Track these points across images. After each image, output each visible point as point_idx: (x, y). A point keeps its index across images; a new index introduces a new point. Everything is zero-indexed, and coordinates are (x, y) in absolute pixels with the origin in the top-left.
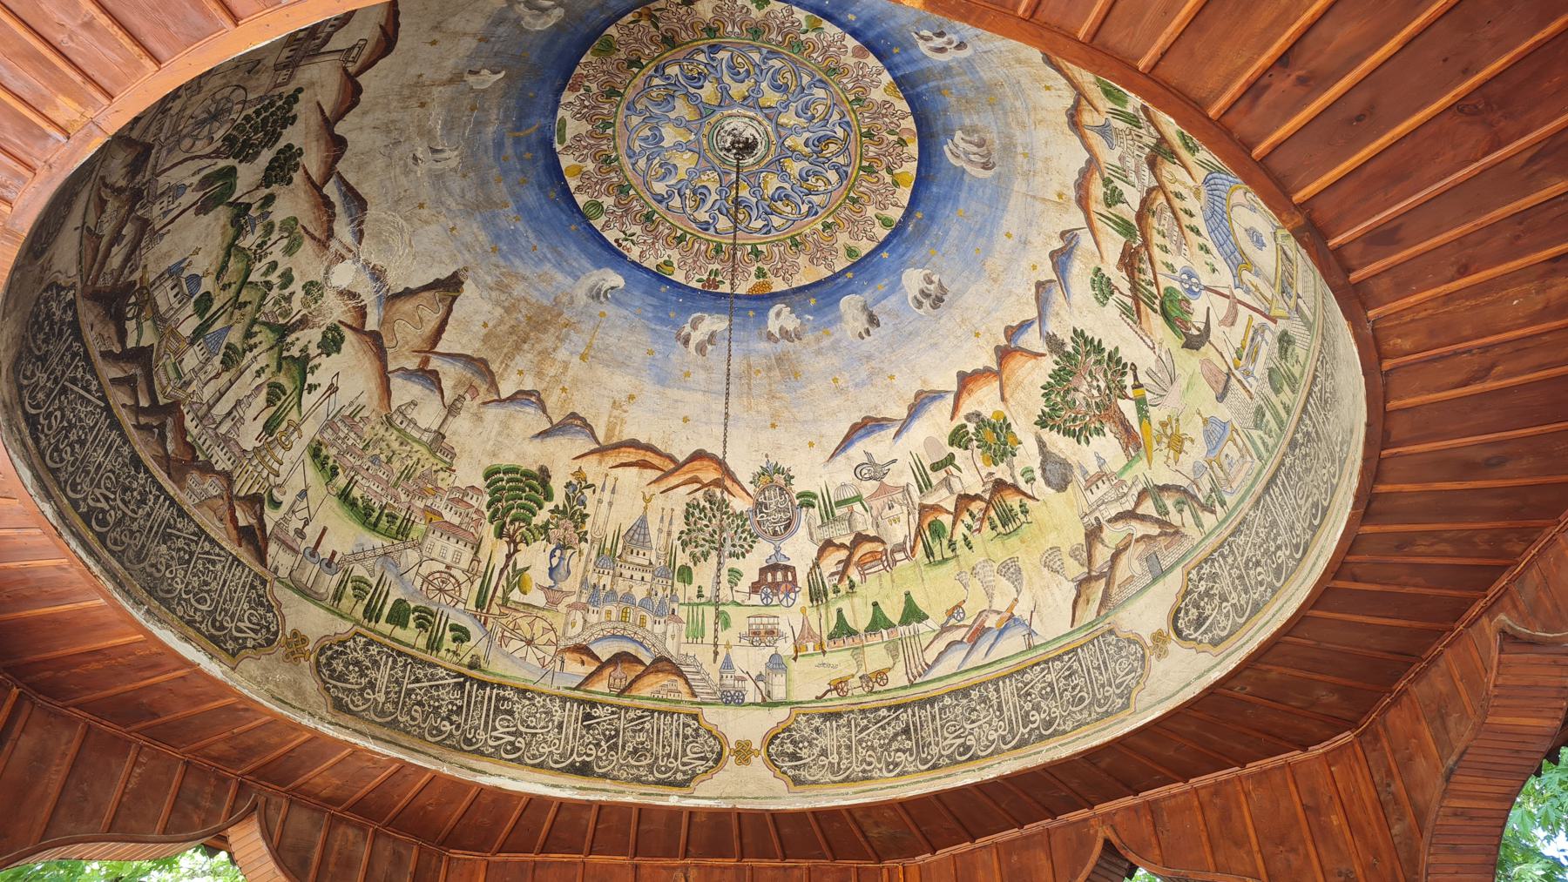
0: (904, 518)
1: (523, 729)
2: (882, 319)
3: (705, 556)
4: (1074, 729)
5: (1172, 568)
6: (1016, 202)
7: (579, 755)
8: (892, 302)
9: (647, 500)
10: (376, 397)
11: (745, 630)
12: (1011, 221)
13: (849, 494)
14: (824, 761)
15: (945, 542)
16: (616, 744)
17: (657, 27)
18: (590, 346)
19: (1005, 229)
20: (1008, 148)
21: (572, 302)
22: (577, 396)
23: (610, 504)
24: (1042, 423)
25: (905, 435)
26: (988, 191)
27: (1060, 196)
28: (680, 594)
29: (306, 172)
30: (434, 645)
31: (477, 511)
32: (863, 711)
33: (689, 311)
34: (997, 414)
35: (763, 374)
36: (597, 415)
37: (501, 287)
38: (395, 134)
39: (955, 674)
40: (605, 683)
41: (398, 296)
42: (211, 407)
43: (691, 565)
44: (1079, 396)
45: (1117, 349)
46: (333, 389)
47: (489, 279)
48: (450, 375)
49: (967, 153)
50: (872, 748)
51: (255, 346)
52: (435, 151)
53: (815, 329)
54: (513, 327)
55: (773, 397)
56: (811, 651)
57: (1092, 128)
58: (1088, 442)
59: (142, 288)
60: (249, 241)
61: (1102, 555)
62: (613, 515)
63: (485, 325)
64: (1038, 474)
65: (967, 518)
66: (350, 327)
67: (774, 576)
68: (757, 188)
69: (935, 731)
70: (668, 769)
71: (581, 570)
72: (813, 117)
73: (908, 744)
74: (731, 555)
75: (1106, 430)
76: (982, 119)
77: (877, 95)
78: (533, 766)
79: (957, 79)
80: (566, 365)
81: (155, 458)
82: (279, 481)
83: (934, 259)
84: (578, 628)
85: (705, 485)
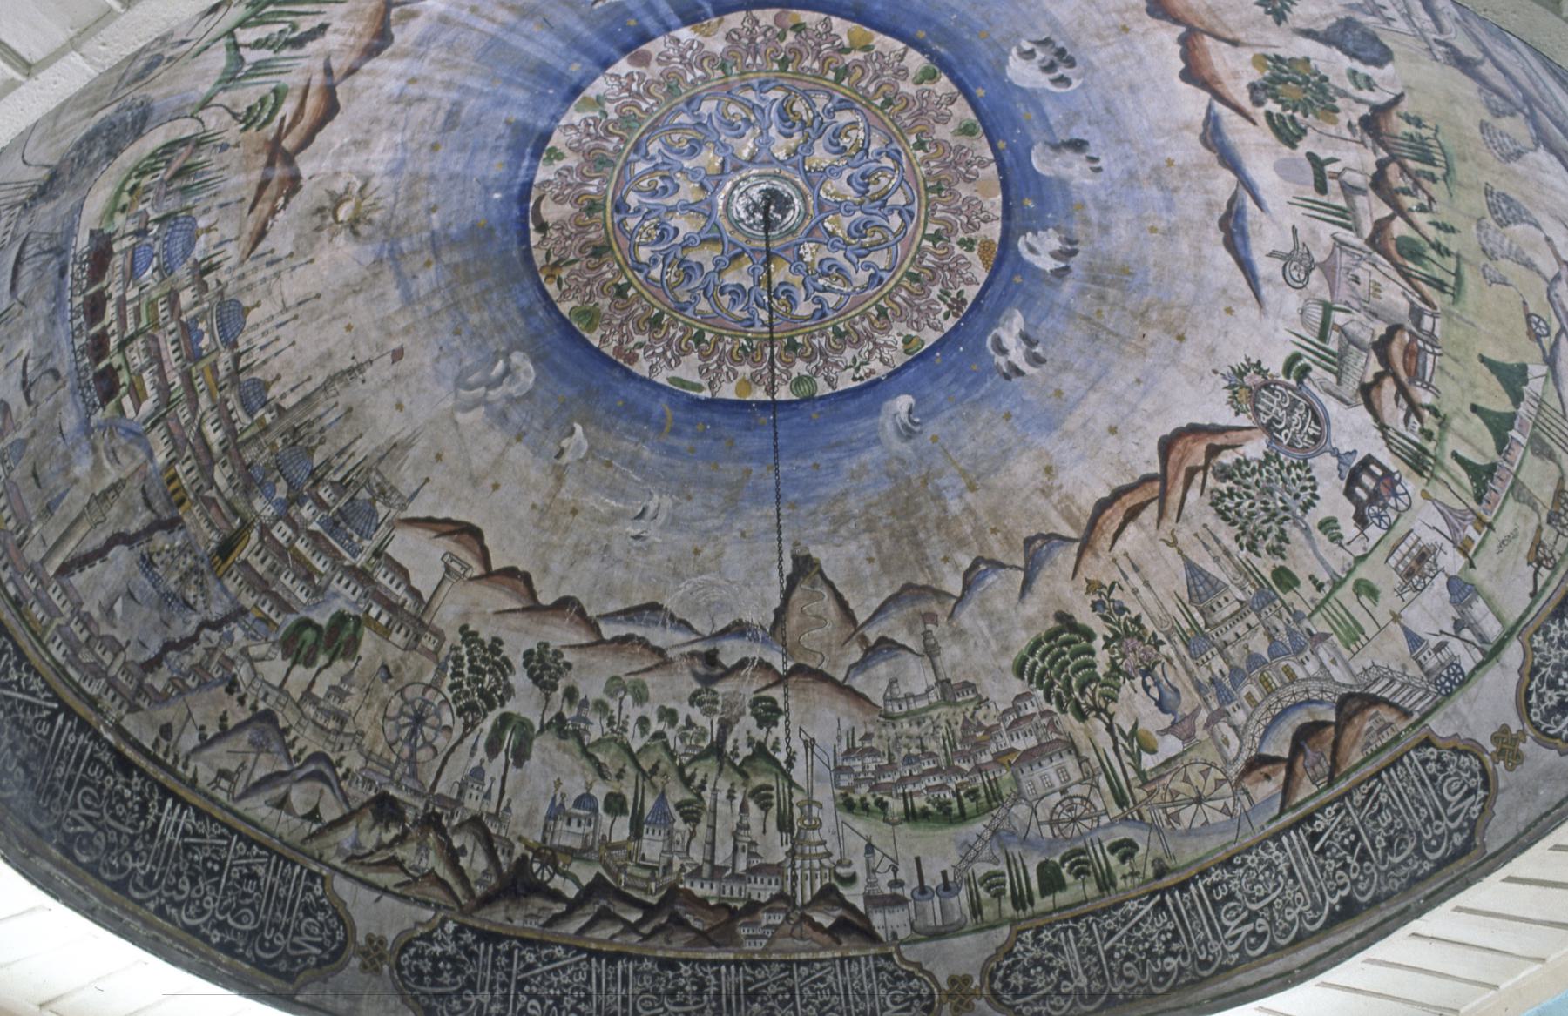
1: (1254, 907)
2: (1076, 133)
3: (1282, 537)
7: (1332, 894)
8: (1055, 115)
9: (1173, 543)
10: (855, 711)
11: (1397, 580)
13: (1316, 313)
15: (1432, 253)
16: (1364, 850)
21: (902, 461)
22: (1010, 523)
23: (1146, 584)
25: (1264, 197)
28: (1299, 606)
30: (1106, 882)
31: (1043, 714)
33: (980, 347)
35: (1105, 309)
36: (1045, 518)
37: (840, 520)
38: (594, 547)
40: (1306, 780)
42: (711, 862)
43: (1280, 562)
46: (810, 744)
47: (823, 528)
48: (895, 627)
51: (704, 782)
52: (640, 516)
53: (1069, 216)
54: (892, 535)
55: (1142, 316)
56: (1477, 538)
60: (596, 729)
62: (1160, 591)
63: (871, 560)
67: (1363, 486)
68: (840, 207)
71: (1185, 677)
72: (747, 121)
74: (1306, 507)
77: (717, 45)
78: (1292, 943)
80: (968, 510)
81: (690, 945)
82: (836, 857)
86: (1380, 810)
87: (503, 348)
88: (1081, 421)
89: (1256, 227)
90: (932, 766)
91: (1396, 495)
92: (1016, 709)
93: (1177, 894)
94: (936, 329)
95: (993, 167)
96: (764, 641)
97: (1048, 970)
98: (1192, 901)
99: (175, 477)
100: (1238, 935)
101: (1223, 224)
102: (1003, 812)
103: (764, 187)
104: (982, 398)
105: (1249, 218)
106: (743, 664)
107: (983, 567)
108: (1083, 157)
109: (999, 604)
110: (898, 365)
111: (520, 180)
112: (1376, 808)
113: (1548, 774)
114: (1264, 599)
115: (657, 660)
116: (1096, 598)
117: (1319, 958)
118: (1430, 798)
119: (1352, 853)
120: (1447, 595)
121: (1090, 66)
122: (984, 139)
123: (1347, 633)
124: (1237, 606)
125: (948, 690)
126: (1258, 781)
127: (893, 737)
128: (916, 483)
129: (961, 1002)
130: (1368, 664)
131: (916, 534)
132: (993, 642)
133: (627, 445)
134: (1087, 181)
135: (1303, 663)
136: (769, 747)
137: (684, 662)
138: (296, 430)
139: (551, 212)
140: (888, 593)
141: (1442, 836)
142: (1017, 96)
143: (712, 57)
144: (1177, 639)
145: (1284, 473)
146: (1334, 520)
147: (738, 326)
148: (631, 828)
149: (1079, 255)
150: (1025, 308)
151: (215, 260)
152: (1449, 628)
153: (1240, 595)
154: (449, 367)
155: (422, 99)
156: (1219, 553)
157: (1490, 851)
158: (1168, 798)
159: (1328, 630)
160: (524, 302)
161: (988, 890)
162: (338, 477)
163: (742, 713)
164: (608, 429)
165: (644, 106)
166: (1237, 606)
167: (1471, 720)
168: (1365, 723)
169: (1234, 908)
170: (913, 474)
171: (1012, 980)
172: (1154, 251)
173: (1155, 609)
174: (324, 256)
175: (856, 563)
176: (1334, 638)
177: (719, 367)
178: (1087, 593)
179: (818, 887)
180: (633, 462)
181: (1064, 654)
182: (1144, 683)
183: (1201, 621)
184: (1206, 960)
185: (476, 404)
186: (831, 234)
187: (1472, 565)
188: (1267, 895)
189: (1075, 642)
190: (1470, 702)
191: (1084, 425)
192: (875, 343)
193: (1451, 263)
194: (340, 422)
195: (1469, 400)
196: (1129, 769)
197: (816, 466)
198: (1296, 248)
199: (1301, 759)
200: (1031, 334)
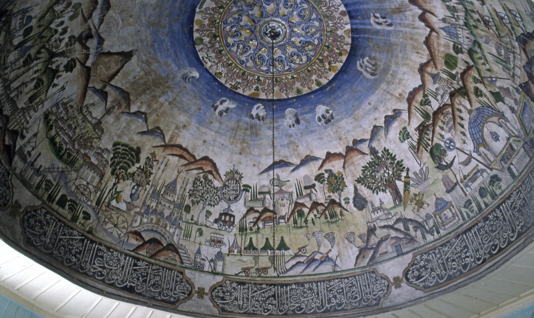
1: (106, 266)
2: (302, 122)
3: (198, 202)
4: (351, 309)
5: (407, 253)
8: (308, 116)
9: (179, 173)
10: (79, 97)
11: (209, 238)
12: (373, 99)
13: (266, 190)
14: (236, 303)
15: (303, 220)
16: (146, 280)
18: (175, 99)
20: (386, 70)
21: (174, 78)
22: (162, 119)
23: (163, 171)
24: (358, 181)
25: (296, 172)
27: (400, 95)
30: (75, 219)
31: (106, 161)
32: (255, 284)
34: (339, 173)
37: (148, 63)
39: (298, 276)
40: (145, 251)
41: (104, 54)
43: (191, 205)
44: (378, 175)
45: (402, 161)
46: (63, 88)
47: (144, 58)
49: (366, 67)
50: (258, 301)
51: (39, 58)
54: (145, 82)
55: (244, 141)
58: (377, 193)
59: (9, 14)
60: (58, 8)
61: (374, 240)
62: (163, 175)
63: (135, 78)
64: (351, 201)
65: (315, 212)
67: (225, 218)
69: (287, 299)
70: (167, 295)
71: (144, 197)
72: (309, 32)
73: (274, 302)
74: (209, 204)
75: (387, 191)
76: (382, 58)
77: (340, 32)
79: (379, 37)
80: (162, 105)
82: (28, 126)
83: (333, 104)
84: (138, 223)
85: (204, 172)
86: (158, 275)
88: (205, 132)
89: (284, 170)
90: (71, 135)
91: (229, 227)
92: (103, 151)
93: (89, 242)
94: (226, 82)
95: (286, 97)
96: (96, 52)
97: (42, 228)
98: (91, 248)
100: (96, 269)
101: (281, 161)
102: (70, 169)
103: (281, 33)
104: (204, 100)
105: (287, 168)
106: (87, 48)
107: (143, 116)
108: (294, 123)
109: (133, 127)
110: (211, 71)
112: (157, 274)
113: (207, 307)
114: (179, 206)
116: (150, 157)
117: (113, 294)
118: (172, 285)
119: (142, 278)
121: (326, 128)
122: (296, 96)
123: (186, 234)
124: (172, 200)
125: (98, 125)
126: (134, 238)
127: (75, 116)
128: (167, 85)
129: (14, 212)
130: (184, 244)
131: (148, 89)
132: (120, 131)
134: (285, 124)
135: (171, 227)
136: (58, 74)
137: (86, 27)
140: (123, 88)
142: (312, 107)
143: (337, 29)
144: (153, 188)
145: (215, 195)
146: (211, 214)
147: (224, 19)
148: (19, 44)
149: (259, 121)
150: (237, 107)
152: (209, 259)
153: (176, 199)
156: (184, 187)
157: (178, 309)
158: (109, 217)
159: (184, 228)
161: (46, 185)
163: (68, 57)
165: (323, 8)
166: (172, 200)
167: (197, 279)
168: (171, 255)
169: (101, 261)
170: (170, 82)
171: (31, 220)
173: (157, 177)
176: (183, 232)
177: (208, 14)
178: (151, 154)
179: (16, 128)
181: (128, 156)
182: (134, 186)
183: (162, 192)
184: (83, 267)
186: (260, 50)
187: (228, 255)
188: (112, 266)
189: (133, 158)
190: (199, 276)
192: (217, 63)
193: (304, 225)
196: (108, 198)
197: (168, 50)
198: (283, 182)
199: (149, 245)
200: (229, 111)
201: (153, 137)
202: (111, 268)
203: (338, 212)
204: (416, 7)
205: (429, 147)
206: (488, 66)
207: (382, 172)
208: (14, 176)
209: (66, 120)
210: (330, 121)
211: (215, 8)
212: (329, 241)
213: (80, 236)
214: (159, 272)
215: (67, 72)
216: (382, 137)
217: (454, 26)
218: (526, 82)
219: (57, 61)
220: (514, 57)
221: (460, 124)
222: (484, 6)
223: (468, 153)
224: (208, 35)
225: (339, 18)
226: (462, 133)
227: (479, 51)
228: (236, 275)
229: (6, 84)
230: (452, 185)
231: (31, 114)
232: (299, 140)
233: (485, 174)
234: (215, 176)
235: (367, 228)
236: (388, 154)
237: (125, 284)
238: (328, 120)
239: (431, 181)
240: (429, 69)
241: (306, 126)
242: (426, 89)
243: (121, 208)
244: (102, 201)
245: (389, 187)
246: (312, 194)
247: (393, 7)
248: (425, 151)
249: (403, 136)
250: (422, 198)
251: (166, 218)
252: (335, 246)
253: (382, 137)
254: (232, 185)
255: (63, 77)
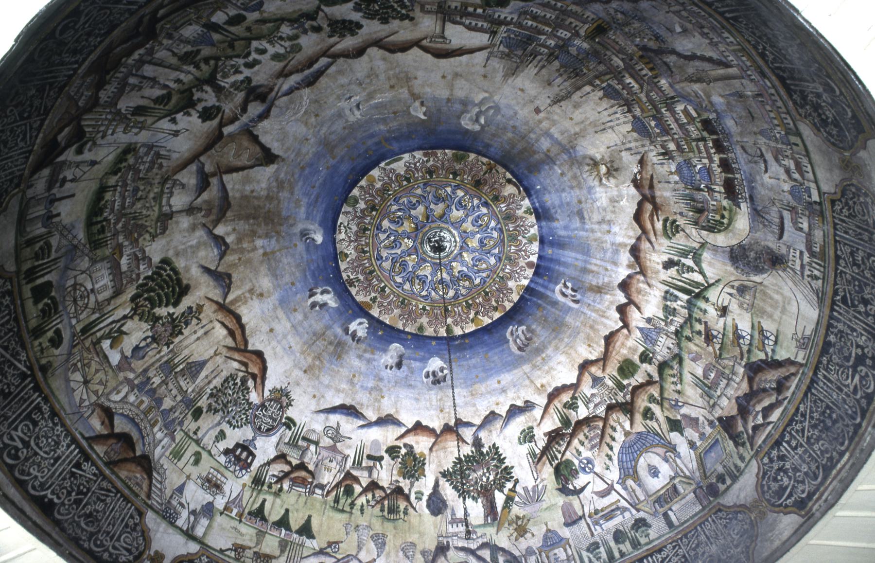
0: (334, 471)
1: (32, 443)
2: (404, 368)
3: (216, 411)
6: (517, 373)
7: (53, 493)
8: (416, 365)
9: (216, 354)
10: (179, 162)
11: (204, 474)
12: (506, 378)
13: (314, 437)
15: (349, 501)
16: (81, 500)
17: (485, 174)
18: (273, 253)
19: (499, 378)
20: (538, 351)
21: (292, 225)
22: (241, 268)
23: (198, 339)
24: (444, 474)
25: (365, 430)
26: (509, 358)
27: (542, 386)
28: (186, 423)
29: (338, 43)
30: (38, 332)
31: (138, 275)
34: (422, 454)
36: (239, 287)
37: (281, 185)
40: (105, 448)
43: (205, 410)
44: (473, 476)
45: (512, 467)
47: (282, 175)
48: (212, 193)
49: (518, 337)
52: (358, 106)
53: (370, 345)
54: (259, 206)
55: (318, 357)
56: (233, 514)
57: (591, 374)
62: (194, 346)
63: (252, 191)
64: (425, 498)
65: (370, 496)
66: (222, 118)
72: (477, 266)
74: (229, 422)
75: (480, 500)
76: (542, 334)
77: (511, 284)
79: (553, 310)
80: (255, 249)
84: (117, 398)
86: (102, 501)
87: (486, 128)
88: (280, 317)
91: (241, 470)
92: (144, 259)
93: (32, 385)
96: (247, 125)
98: (29, 398)
99: (651, 69)
102: (86, 251)
104: (306, 276)
105: (355, 420)
106: (244, 110)
107: (223, 248)
109: (202, 253)
111: (534, 197)
112: (103, 498)
115: (285, 72)
116: (194, 309)
117: (13, 503)
119: (77, 494)
120: (205, 504)
121: (430, 389)
125: (166, 218)
126: (100, 418)
127: (153, 182)
130: (165, 467)
131: (254, 218)
133: (394, 125)
134: (382, 361)
137: (271, 84)
138: (577, 75)
139: (510, 190)
140: (230, 194)
141: (103, 546)
142: (427, 355)
143: (510, 279)
144: (170, 356)
146: (225, 438)
151: (661, 157)
152: (192, 507)
153: (190, 390)
154: (504, 111)
155: (599, 223)
156: (210, 378)
158: (86, 361)
159: (177, 441)
160: (492, 149)
161: (41, 248)
162: (539, 57)
163: (218, 100)
164: (408, 125)
166: (185, 389)
169: (29, 429)
170: (284, 228)
172: (344, 372)
174: (603, 149)
175: (255, 184)
176: (174, 445)
177: (389, 177)
179: (87, 130)
180: (384, 121)
181: (168, 288)
182: (148, 337)
183: (178, 369)
185: (482, 103)
186: (409, 255)
187: (221, 513)
188: (40, 448)
189: (173, 295)
190: (165, 532)
191: (277, 318)
193: (347, 509)
194: (552, 79)
195: (290, 508)
196: (102, 332)
197: (314, 187)
199: (115, 441)
201: (215, 283)
202: (38, 450)
203: (402, 507)
204: (622, 294)
205: (556, 462)
206: (679, 387)
207: (480, 473)
208: (20, 195)
209: (139, 179)
210: (439, 383)
211: (402, 176)
212: (376, 545)
213: (26, 366)
214: (107, 496)
215: (199, 117)
216: (496, 429)
217: (659, 331)
218: (732, 416)
219: (206, 92)
220: (727, 385)
221: (608, 445)
222: (722, 320)
223: (610, 482)
224: (369, 201)
225: (522, 267)
226: (607, 455)
227: (676, 366)
228: (222, 551)
229: (145, 58)
230: (575, 518)
231: (118, 130)
232: (389, 390)
233: (627, 515)
234: (257, 385)
235: (436, 544)
236: (497, 453)
237: (44, 493)
238: (437, 381)
239: (544, 505)
240: (593, 369)
241: (407, 375)
242: (579, 390)
243: (111, 360)
244: (92, 331)
245: (484, 496)
246: (375, 470)
247: (594, 283)
248: (549, 465)
249: (525, 437)
250: (526, 524)
251: (162, 412)
252: (383, 557)
253: (496, 429)
254: (272, 410)
255: (190, 119)
